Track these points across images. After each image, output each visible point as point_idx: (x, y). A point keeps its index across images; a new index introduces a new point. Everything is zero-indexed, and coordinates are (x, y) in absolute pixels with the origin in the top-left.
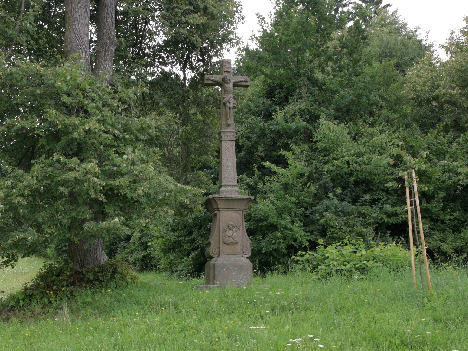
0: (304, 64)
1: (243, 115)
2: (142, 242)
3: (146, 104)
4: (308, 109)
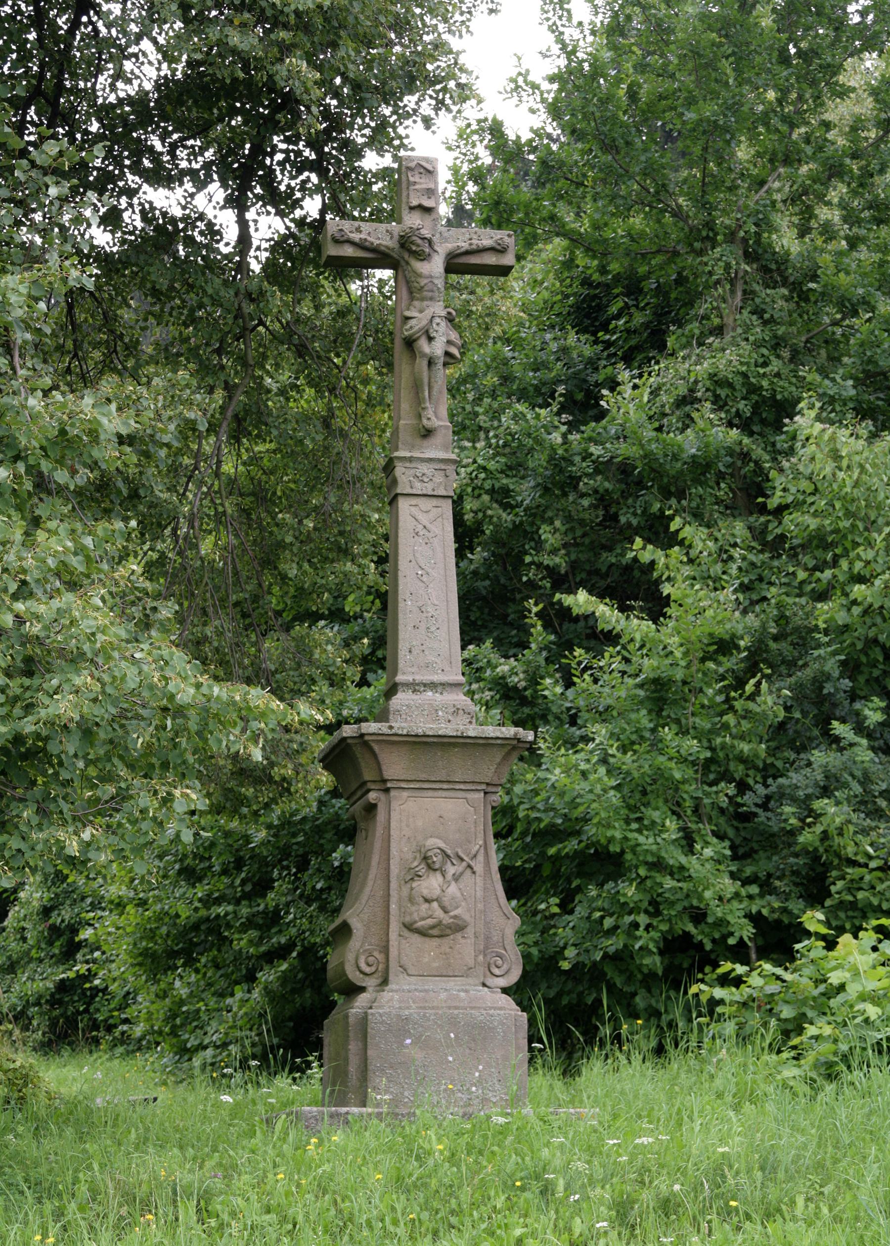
0: (730, 189)
1: (478, 400)
2: (53, 929)
3: (84, 340)
4: (745, 375)
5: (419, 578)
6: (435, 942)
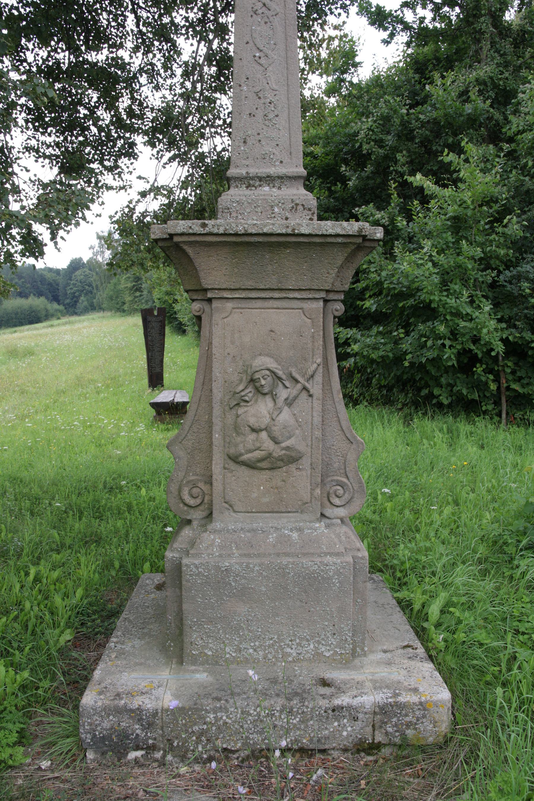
4: (491, 78)
5: (257, 60)
6: (265, 475)
